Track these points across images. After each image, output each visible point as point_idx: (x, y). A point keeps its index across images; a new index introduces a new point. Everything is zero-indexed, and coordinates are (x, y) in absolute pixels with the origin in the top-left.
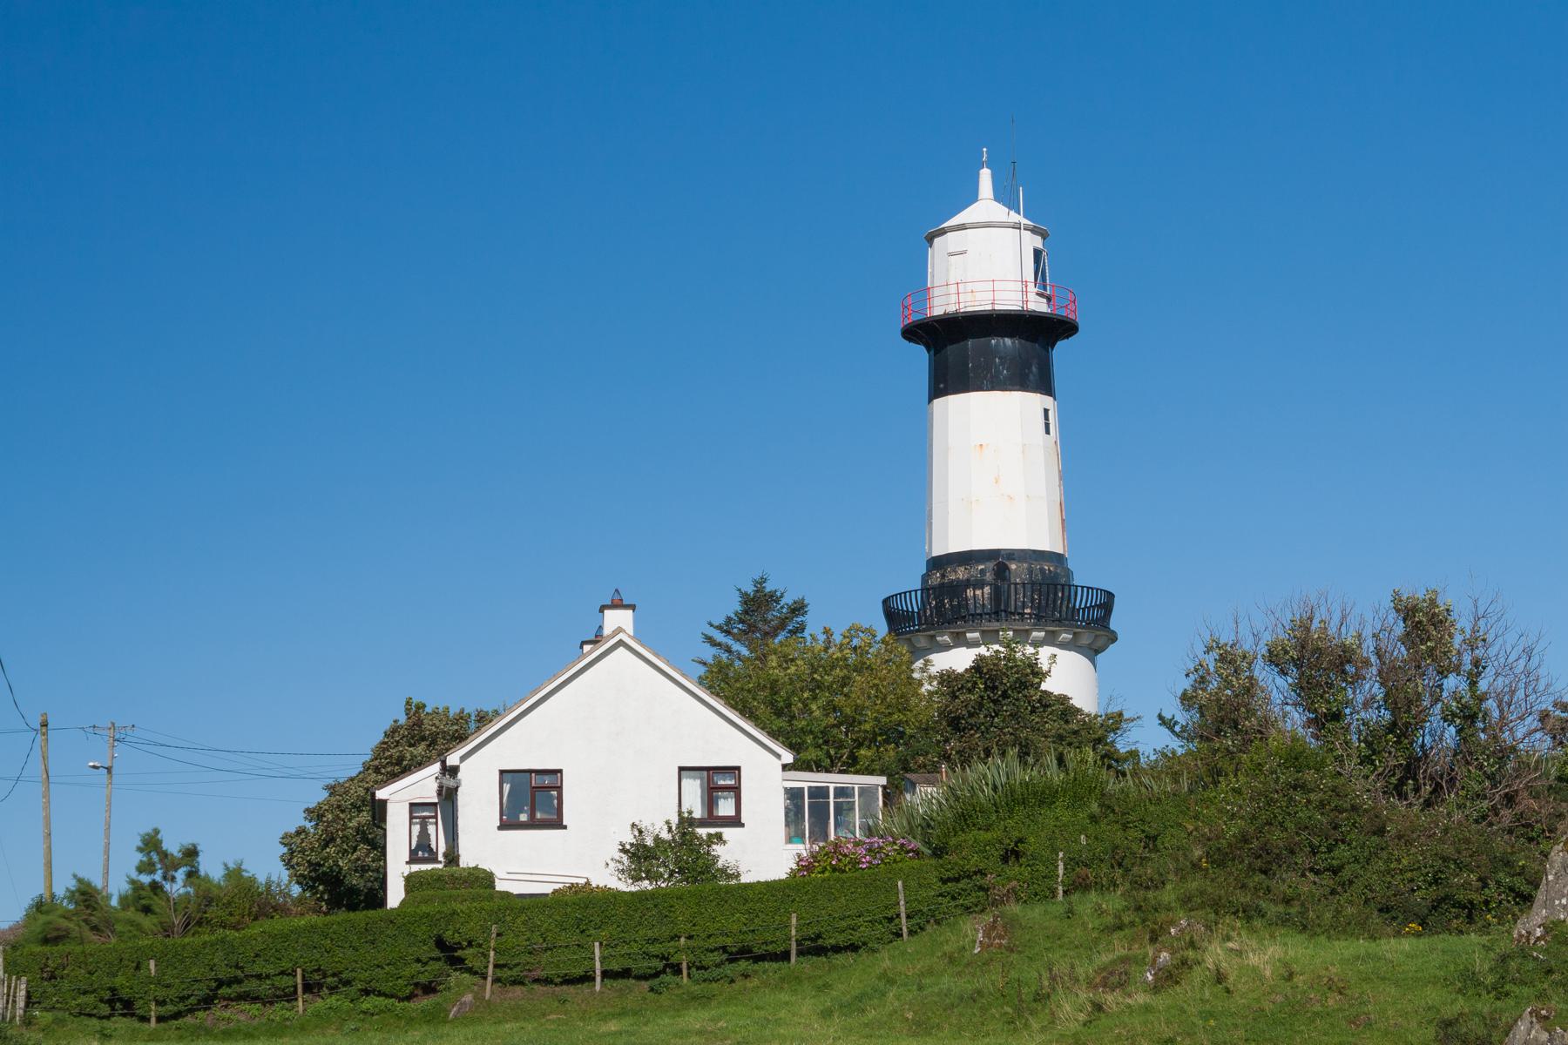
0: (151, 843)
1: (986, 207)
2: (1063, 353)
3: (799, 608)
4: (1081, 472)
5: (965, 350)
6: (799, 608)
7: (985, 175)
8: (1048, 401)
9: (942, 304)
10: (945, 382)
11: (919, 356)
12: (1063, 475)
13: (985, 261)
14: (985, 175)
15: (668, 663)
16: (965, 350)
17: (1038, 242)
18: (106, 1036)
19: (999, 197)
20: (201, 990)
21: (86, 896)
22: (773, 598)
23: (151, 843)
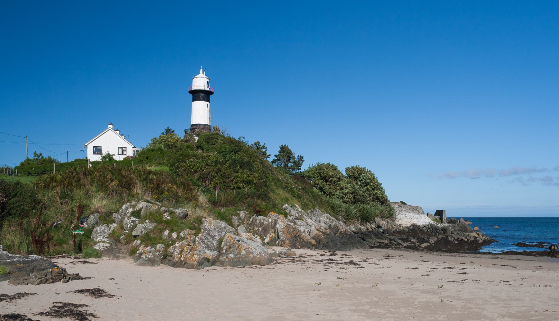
0: (35, 153)
1: (201, 74)
2: (211, 96)
3: (173, 132)
4: (213, 114)
5: (197, 95)
6: (173, 132)
7: (201, 70)
8: (208, 103)
9: (193, 89)
10: (194, 99)
11: (191, 96)
12: (210, 114)
13: (200, 82)
14: (201, 70)
15: (100, 133)
16: (197, 95)
17: (208, 80)
18: (440, 213)
19: (203, 73)
20: (40, 172)
21: (28, 159)
22: (170, 130)
23: (35, 153)
